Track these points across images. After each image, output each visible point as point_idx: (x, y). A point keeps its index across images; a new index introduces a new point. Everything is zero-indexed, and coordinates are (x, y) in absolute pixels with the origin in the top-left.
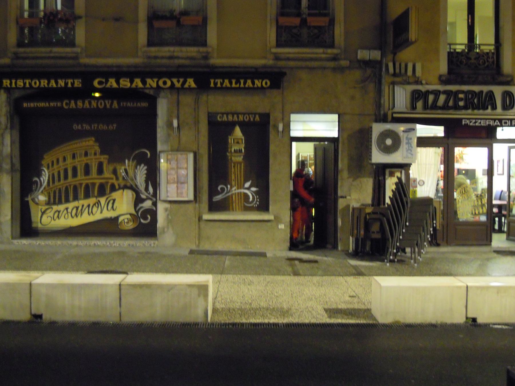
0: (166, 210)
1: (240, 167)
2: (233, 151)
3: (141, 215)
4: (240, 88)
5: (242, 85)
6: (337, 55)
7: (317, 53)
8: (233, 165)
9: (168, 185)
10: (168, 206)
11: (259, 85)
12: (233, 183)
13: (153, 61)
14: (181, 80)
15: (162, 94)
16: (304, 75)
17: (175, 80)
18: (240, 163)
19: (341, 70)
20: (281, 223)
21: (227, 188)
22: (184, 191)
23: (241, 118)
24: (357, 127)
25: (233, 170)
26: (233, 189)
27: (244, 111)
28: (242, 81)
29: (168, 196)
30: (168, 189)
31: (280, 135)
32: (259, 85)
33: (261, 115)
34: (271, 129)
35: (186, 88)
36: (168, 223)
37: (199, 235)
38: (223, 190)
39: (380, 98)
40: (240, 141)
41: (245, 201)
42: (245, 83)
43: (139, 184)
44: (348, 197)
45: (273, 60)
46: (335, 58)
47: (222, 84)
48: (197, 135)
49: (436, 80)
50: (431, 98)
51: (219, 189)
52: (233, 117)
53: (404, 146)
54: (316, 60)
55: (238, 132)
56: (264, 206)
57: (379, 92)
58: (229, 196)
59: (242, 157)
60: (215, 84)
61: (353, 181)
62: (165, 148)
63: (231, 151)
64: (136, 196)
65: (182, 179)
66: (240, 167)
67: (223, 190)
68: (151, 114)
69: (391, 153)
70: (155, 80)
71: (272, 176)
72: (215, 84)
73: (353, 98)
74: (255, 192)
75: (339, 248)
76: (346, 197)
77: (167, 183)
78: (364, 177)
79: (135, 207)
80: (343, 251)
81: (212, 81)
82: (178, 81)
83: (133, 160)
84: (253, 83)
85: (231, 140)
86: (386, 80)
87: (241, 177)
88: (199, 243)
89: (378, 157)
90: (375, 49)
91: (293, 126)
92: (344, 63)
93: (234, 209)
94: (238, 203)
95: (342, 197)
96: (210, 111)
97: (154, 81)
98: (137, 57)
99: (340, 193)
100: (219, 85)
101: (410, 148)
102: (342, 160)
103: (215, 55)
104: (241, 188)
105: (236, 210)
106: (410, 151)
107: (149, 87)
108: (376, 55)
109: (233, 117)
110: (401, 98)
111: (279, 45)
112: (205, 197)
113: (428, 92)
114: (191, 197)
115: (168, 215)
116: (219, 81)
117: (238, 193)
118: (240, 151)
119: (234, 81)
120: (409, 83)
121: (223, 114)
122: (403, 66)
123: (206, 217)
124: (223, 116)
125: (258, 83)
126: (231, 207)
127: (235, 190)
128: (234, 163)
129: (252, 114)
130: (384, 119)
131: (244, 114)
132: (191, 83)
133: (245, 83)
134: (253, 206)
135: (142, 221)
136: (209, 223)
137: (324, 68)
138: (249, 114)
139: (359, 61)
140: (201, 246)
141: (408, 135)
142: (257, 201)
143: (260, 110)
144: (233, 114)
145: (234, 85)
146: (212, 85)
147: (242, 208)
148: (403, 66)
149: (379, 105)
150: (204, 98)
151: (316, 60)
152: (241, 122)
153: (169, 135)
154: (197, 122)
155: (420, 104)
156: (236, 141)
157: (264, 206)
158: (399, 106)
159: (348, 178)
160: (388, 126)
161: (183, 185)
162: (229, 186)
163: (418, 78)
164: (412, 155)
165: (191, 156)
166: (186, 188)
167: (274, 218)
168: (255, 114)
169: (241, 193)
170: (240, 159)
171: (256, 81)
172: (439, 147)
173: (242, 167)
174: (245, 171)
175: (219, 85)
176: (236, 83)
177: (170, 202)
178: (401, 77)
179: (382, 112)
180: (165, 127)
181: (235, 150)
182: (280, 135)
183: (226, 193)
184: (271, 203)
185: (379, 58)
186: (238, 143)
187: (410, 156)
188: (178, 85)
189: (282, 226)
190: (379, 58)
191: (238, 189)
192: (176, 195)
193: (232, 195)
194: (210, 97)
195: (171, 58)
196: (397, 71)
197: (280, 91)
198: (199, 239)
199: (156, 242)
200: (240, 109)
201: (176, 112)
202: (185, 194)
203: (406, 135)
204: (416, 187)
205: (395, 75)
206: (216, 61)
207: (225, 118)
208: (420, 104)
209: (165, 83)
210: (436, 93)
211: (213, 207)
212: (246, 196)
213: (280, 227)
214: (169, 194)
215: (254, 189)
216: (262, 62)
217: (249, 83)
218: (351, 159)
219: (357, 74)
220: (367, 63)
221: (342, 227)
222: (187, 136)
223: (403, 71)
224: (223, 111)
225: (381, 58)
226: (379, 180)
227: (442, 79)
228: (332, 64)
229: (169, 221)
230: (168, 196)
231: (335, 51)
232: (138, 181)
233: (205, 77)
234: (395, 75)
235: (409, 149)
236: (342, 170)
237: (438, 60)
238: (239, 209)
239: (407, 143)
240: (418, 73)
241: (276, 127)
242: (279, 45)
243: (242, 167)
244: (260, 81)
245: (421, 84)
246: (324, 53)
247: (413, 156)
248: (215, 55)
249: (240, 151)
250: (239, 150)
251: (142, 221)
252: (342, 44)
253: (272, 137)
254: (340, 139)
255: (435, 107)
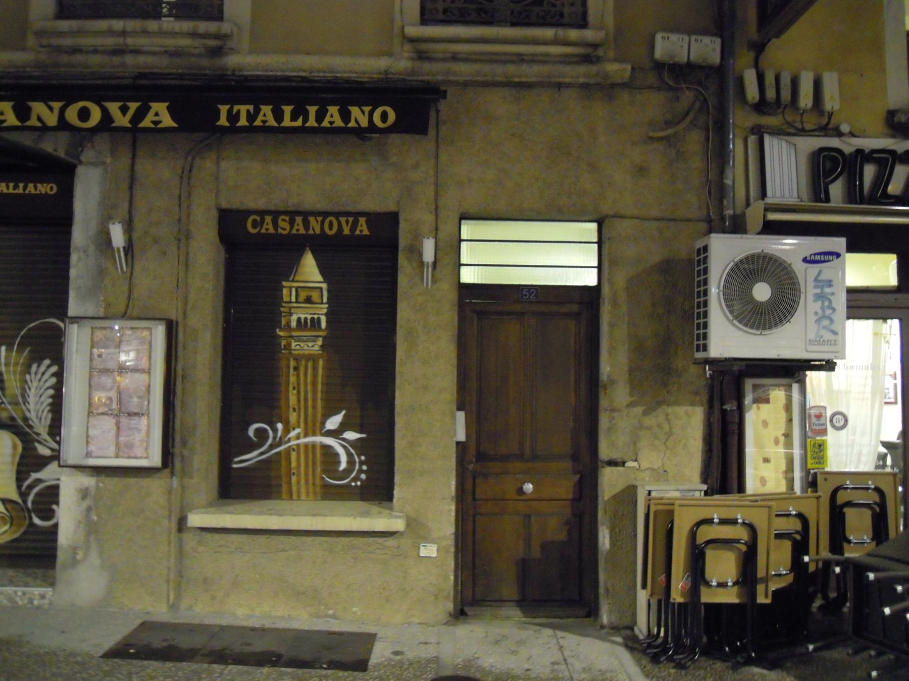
0: (84, 493)
1: (315, 369)
2: (294, 324)
3: (33, 502)
4: (303, 130)
5: (312, 122)
6: (595, 46)
7: (535, 42)
8: (292, 363)
9: (93, 421)
10: (88, 481)
11: (364, 123)
12: (293, 417)
13: (65, 58)
14: (133, 106)
15: (88, 155)
16: (498, 103)
17: (114, 107)
18: (313, 358)
19: (606, 89)
20: (427, 540)
21: (275, 430)
22: (138, 437)
23: (315, 226)
24: (656, 256)
25: (293, 379)
26: (293, 434)
27: (324, 206)
28: (312, 110)
29: (88, 455)
30: (91, 432)
31: (428, 273)
32: (364, 123)
33: (373, 218)
34: (402, 260)
35: (146, 130)
36: (88, 534)
37: (180, 574)
38: (261, 434)
39: (722, 173)
40: (315, 296)
41: (325, 471)
42: (320, 117)
43: (32, 415)
44: (630, 464)
45: (412, 59)
46: (589, 56)
47: (251, 117)
48: (182, 274)
49: (879, 125)
50: (869, 172)
51: (251, 433)
52: (292, 223)
53: (808, 306)
54: (533, 60)
55: (309, 269)
56: (379, 488)
57: (720, 156)
58: (279, 454)
59: (320, 342)
60: (233, 118)
61: (645, 413)
62: (89, 309)
63: (288, 324)
64: (24, 449)
65: (134, 404)
66: (315, 369)
67: (261, 434)
68: (59, 217)
69: (770, 328)
70: (57, 105)
71: (403, 397)
72: (233, 118)
73: (642, 171)
74: (354, 444)
75: (605, 619)
76: (623, 464)
77: (90, 413)
78: (676, 403)
79: (20, 480)
80: (615, 629)
81: (224, 109)
82: (124, 110)
83: (22, 346)
84: (346, 116)
85: (288, 293)
86: (740, 119)
87: (314, 400)
88: (179, 597)
89: (728, 340)
90: (705, 32)
91: (467, 253)
92: (618, 70)
93: (295, 496)
94: (306, 474)
95: (612, 463)
96: (225, 205)
97: (51, 109)
98: (24, 49)
99: (605, 451)
100: (243, 122)
101: (828, 312)
102: (612, 349)
103: (245, 44)
104: (314, 435)
105: (299, 498)
106: (826, 322)
107: (39, 124)
108: (707, 49)
109: (292, 223)
110: (785, 167)
111: (425, 19)
112: (203, 455)
113: (862, 157)
114: (155, 460)
115: (89, 509)
116: (243, 109)
117: (306, 446)
118: (315, 323)
119: (288, 110)
120: (803, 132)
121: (262, 213)
122: (786, 81)
123: (195, 520)
124: (263, 220)
125: (359, 116)
126: (285, 488)
127: (297, 438)
128: (297, 359)
129: (347, 214)
130: (737, 226)
131: (325, 214)
132: (161, 114)
133: (320, 117)
134: (348, 486)
135: (37, 521)
136: (209, 536)
137: (559, 86)
138: (337, 215)
139: (659, 66)
140: (185, 603)
141: (820, 272)
142: (361, 471)
143: (369, 204)
144: (292, 214)
145: (287, 122)
146: (223, 121)
147: (318, 489)
148: (786, 81)
149: (718, 190)
150: (207, 165)
151: (533, 60)
152: (315, 236)
153: (101, 273)
154: (184, 236)
155: (837, 189)
156: (303, 295)
157: (379, 488)
158: (778, 194)
159: (631, 405)
160: (752, 244)
161: (134, 421)
162: (280, 426)
163: (830, 115)
164: (835, 333)
165: (160, 331)
166: (144, 429)
167: (408, 525)
168: (357, 215)
169: (314, 446)
170: (315, 347)
171: (355, 111)
172: (885, 319)
173: (320, 371)
174: (327, 384)
175: (243, 122)
176: (294, 118)
177: (98, 471)
178: (779, 110)
179: (729, 212)
180: (92, 249)
181: (299, 320)
182: (428, 273)
183: (272, 447)
184: (397, 479)
185: (715, 58)
186: (309, 300)
187: (828, 336)
188: (122, 121)
189: (429, 551)
190: (715, 58)
191: (306, 435)
192: (112, 450)
193: (288, 451)
194: (224, 164)
195: (119, 51)
196: (771, 94)
197: (426, 143)
198: (178, 587)
199: (49, 591)
200: (311, 199)
201: (126, 205)
202: (139, 451)
203: (814, 269)
204: (824, 432)
205: (761, 107)
206: (245, 60)
207: (268, 227)
208: (837, 189)
209: (84, 114)
210: (886, 161)
211: (234, 487)
212: (329, 454)
213: (423, 552)
214: (92, 448)
215: (351, 435)
216: (382, 63)
217: (333, 114)
218: (638, 348)
219: (652, 105)
220: (679, 73)
221: (609, 552)
222: (153, 275)
223: (786, 95)
224: (261, 204)
225: (722, 58)
226: (724, 412)
227: (896, 119)
228: (580, 73)
229: (91, 528)
230: (88, 455)
231: (589, 35)
232: (31, 407)
233: (203, 105)
234: (761, 107)
235: (824, 317)
236: (612, 382)
237: (882, 70)
238: (308, 494)
239: (819, 297)
240: (831, 102)
241: (416, 251)
242: (425, 19)
243: (320, 371)
244: (367, 109)
245: (840, 134)
246: (556, 42)
247: (837, 337)
248: (245, 44)
249: (315, 323)
250: (312, 319)
251: (37, 521)
252: (610, 21)
253: (403, 281)
254: (606, 290)
255: (879, 196)
